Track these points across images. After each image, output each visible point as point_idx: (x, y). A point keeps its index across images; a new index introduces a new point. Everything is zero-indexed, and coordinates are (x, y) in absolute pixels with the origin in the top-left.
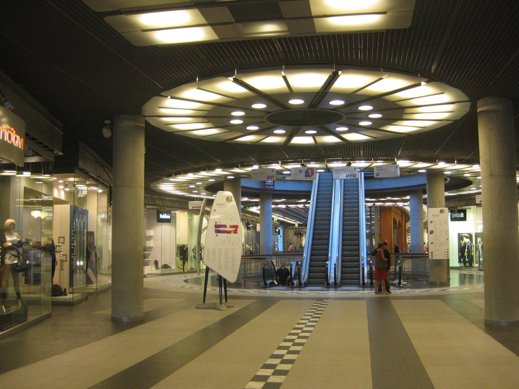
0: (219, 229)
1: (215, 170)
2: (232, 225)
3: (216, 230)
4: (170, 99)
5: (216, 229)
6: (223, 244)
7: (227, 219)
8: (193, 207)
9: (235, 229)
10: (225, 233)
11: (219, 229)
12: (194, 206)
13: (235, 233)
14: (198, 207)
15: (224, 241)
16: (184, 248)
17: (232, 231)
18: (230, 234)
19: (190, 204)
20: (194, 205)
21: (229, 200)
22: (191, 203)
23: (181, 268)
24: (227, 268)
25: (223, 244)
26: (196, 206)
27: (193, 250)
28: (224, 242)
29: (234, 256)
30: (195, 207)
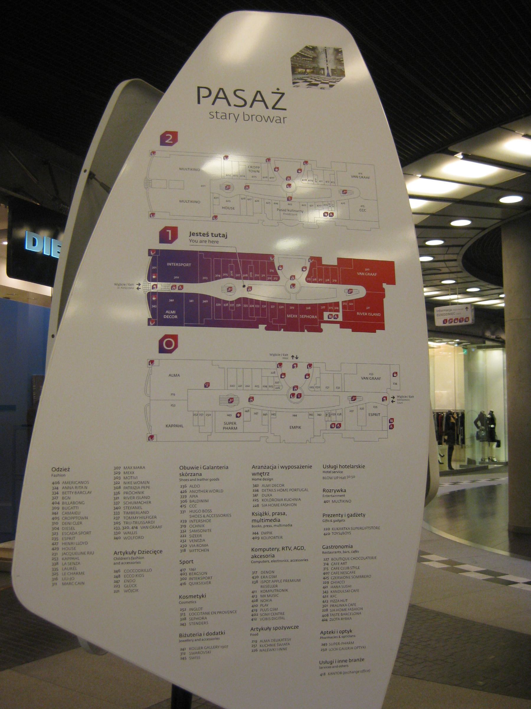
0: (189, 288)
1: (455, 156)
2: (329, 260)
3: (162, 296)
4: (462, 159)
5: (162, 287)
6: (230, 427)
7: (285, 205)
8: (445, 321)
9: (360, 292)
10: (280, 330)
11: (189, 288)
12: (448, 317)
13: (356, 328)
14: (457, 319)
15: (243, 396)
16: (452, 419)
17: (333, 306)
18: (306, 335)
19: (438, 313)
20: (446, 314)
21: (317, 71)
22: (439, 311)
23: (441, 462)
24: (280, 634)
25: (230, 427)
26: (453, 317)
27: (476, 423)
28: (243, 404)
29: (345, 531)
30: (451, 321)
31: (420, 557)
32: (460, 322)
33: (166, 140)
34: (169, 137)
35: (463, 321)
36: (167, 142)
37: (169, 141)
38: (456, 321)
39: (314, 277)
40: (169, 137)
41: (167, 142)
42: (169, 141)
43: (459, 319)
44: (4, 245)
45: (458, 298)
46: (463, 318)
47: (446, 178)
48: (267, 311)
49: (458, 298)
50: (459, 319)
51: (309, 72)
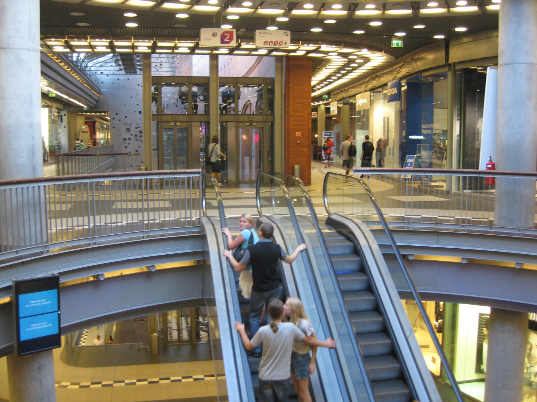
14: (272, 42)
31: (72, 16)
32: (274, 45)
33: (225, 39)
34: (227, 36)
35: (277, 44)
36: (225, 40)
37: (228, 39)
38: (271, 44)
39: (314, 108)
40: (227, 36)
41: (225, 40)
42: (228, 39)
43: (273, 42)
44: (251, 89)
45: (353, 202)
46: (277, 42)
47: (105, 237)
48: (466, 183)
49: (353, 202)
50: (273, 42)
51: (414, 67)
